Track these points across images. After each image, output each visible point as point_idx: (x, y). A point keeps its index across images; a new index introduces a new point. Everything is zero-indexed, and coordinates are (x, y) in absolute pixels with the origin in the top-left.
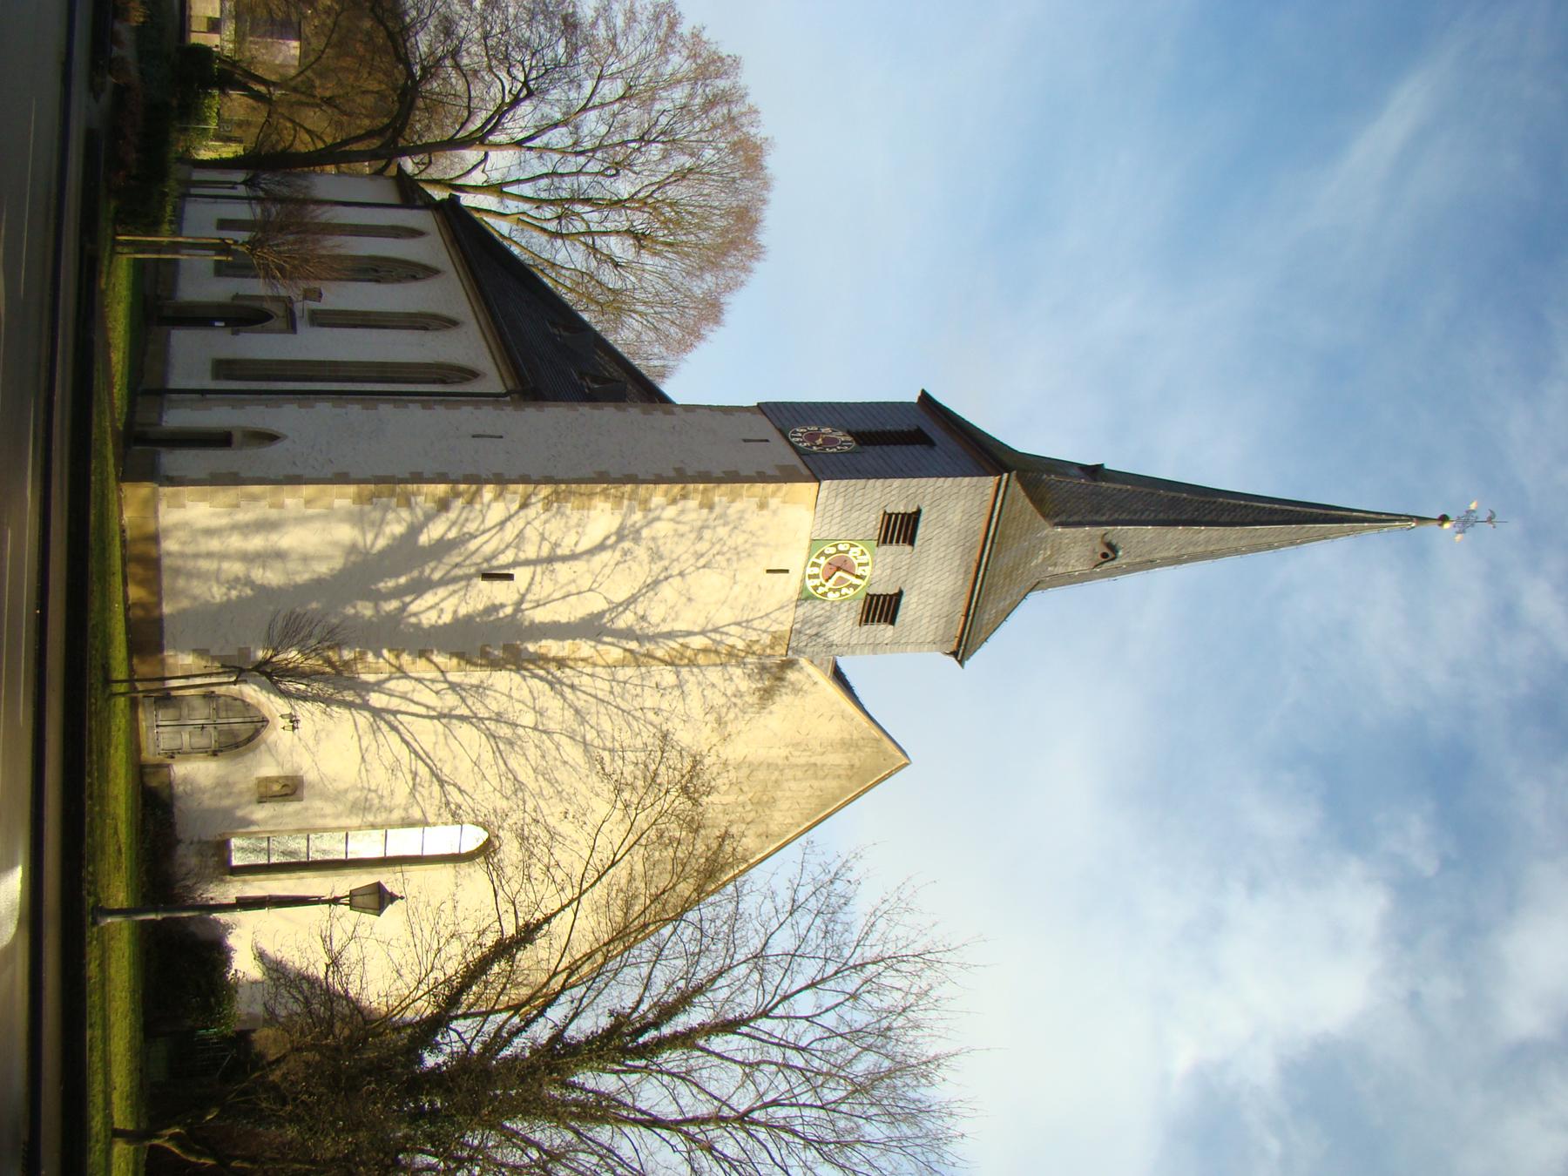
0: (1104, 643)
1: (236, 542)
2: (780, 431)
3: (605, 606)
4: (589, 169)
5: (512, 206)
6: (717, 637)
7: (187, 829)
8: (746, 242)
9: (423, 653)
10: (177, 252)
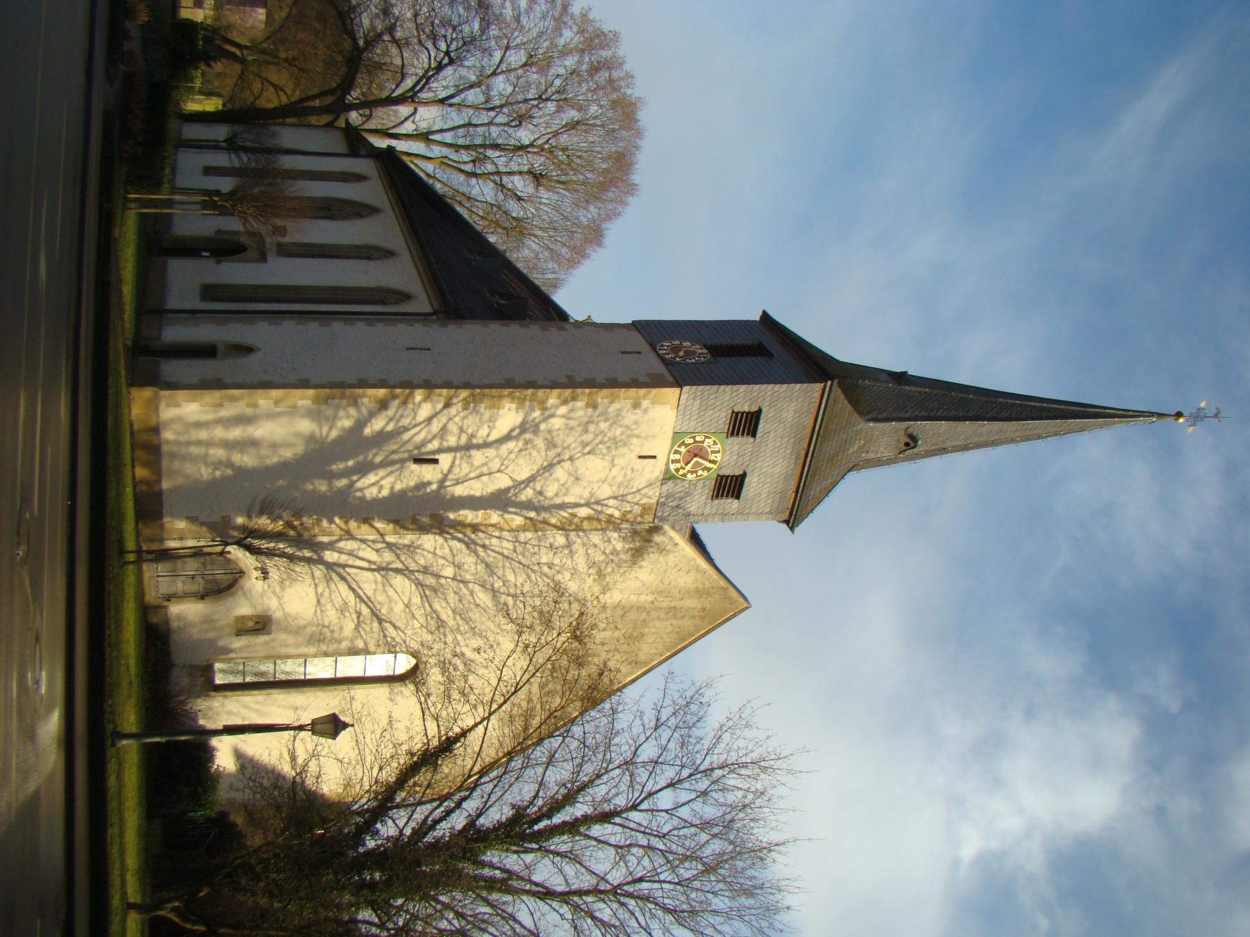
0: (907, 515)
1: (219, 433)
2: (650, 344)
3: (510, 483)
4: (498, 120)
5: (437, 151)
6: (599, 508)
7: (179, 657)
8: (623, 181)
9: (366, 520)
10: (171, 208)
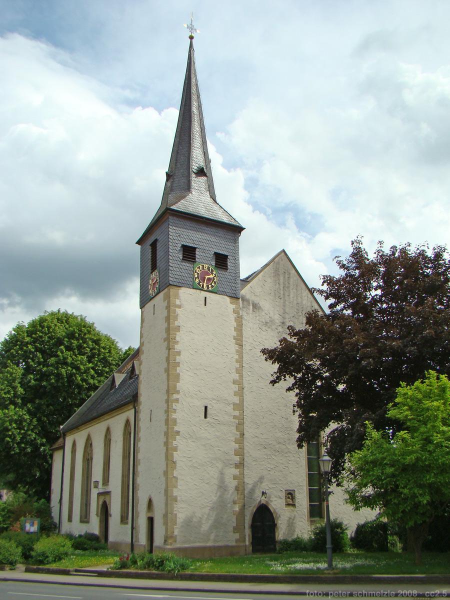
2: (151, 300)
